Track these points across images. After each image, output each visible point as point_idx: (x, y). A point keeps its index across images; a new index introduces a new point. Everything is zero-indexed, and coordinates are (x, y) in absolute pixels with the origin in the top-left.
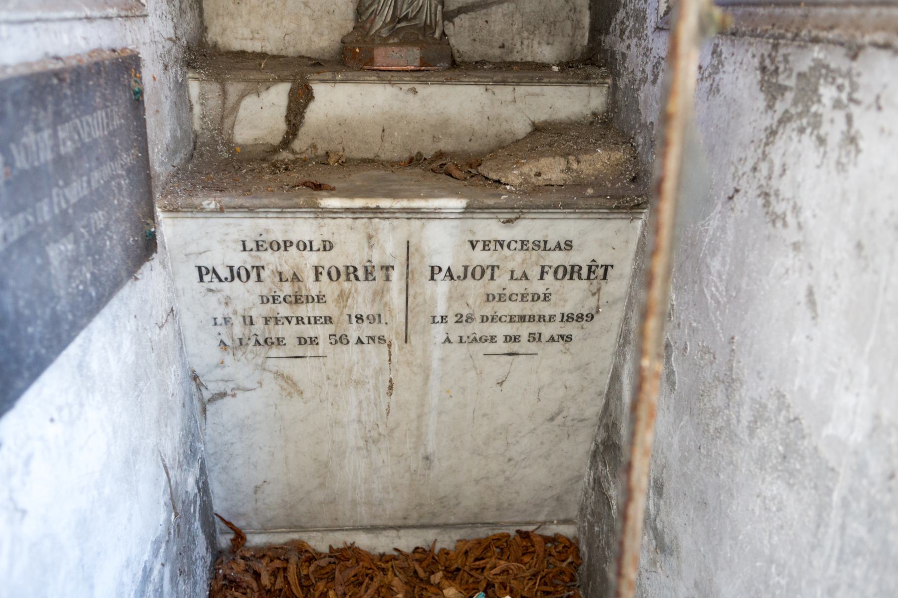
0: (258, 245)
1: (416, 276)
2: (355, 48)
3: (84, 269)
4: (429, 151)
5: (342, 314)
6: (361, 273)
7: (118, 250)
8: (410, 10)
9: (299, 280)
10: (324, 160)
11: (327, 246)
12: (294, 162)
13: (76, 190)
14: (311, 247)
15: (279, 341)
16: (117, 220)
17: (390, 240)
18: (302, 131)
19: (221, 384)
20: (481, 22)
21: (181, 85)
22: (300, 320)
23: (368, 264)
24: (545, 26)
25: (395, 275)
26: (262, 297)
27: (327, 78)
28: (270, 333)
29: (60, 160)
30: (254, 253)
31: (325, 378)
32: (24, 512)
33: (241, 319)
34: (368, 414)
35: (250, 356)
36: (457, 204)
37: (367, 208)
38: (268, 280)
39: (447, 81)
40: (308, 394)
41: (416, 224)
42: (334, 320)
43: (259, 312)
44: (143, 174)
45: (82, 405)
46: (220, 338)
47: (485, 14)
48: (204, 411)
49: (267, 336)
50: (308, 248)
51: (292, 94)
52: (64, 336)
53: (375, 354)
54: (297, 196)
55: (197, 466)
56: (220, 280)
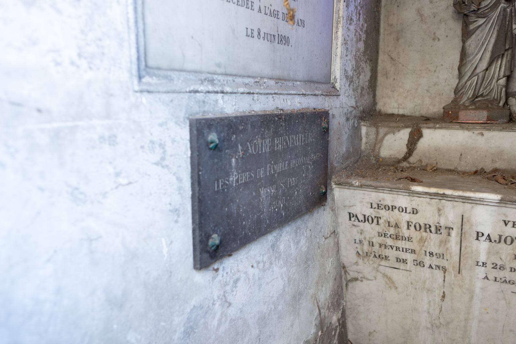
0: (378, 206)
1: (467, 236)
2: (449, 112)
3: (280, 202)
4: (489, 166)
5: (421, 249)
6: (433, 229)
7: (302, 197)
8: (485, 91)
9: (398, 227)
10: (424, 169)
11: (415, 212)
12: (408, 168)
13: (280, 167)
14: (406, 211)
15: (386, 258)
16: (303, 183)
17: (451, 213)
18: (415, 152)
19: (356, 273)
21: (357, 127)
22: (398, 249)
23: (438, 225)
25: (454, 233)
26: (379, 233)
27: (430, 126)
28: (382, 252)
29: (273, 153)
30: (376, 210)
31: (410, 284)
32: (230, 304)
33: (368, 242)
34: (434, 310)
35: (371, 262)
36: (495, 197)
37: (438, 194)
38: (382, 225)
39: (503, 129)
40: (400, 289)
41: (468, 206)
42: (417, 252)
43: (377, 240)
44: (323, 165)
45: (271, 264)
46: (357, 250)
48: (347, 285)
49: (380, 253)
50: (404, 211)
51: (411, 134)
52: (263, 230)
53: (438, 274)
54: (400, 184)
55: (340, 312)
56: (359, 221)
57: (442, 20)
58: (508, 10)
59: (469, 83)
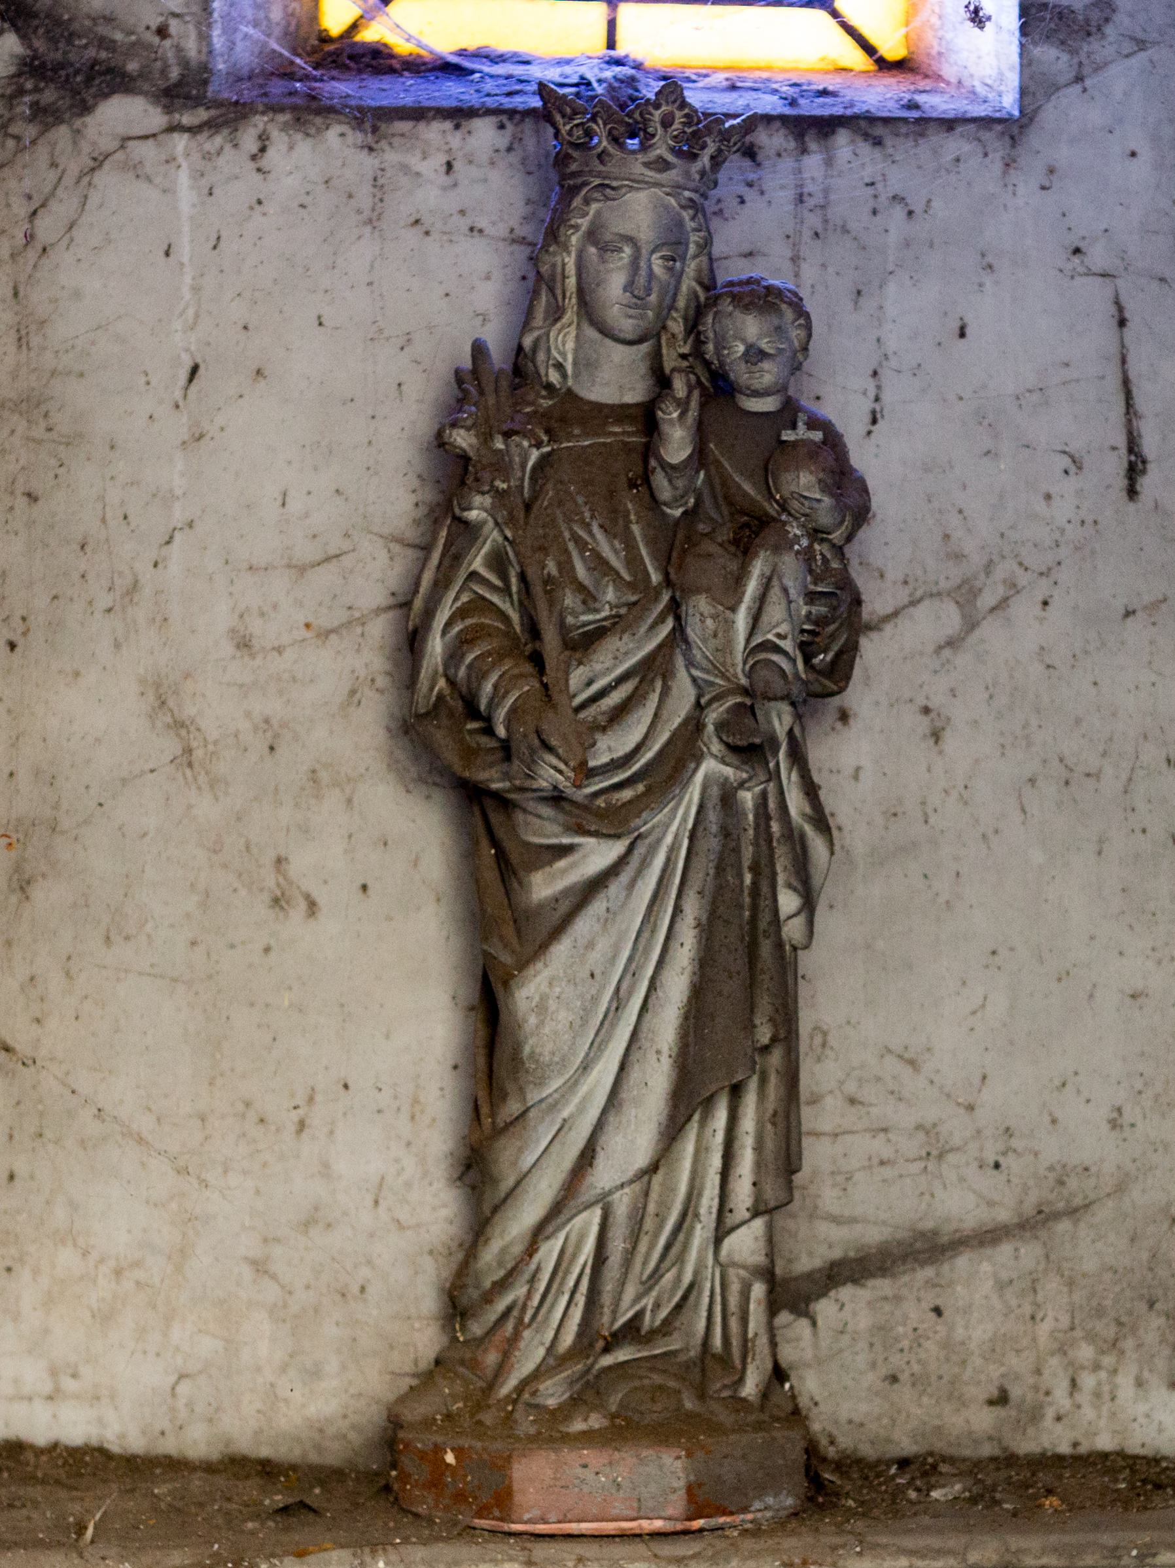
2: (439, 1450)
8: (648, 1301)
20: (915, 1312)
24: (1157, 1322)
47: (931, 1284)
57: (324, 775)
58: (747, 798)
59: (549, 1252)
